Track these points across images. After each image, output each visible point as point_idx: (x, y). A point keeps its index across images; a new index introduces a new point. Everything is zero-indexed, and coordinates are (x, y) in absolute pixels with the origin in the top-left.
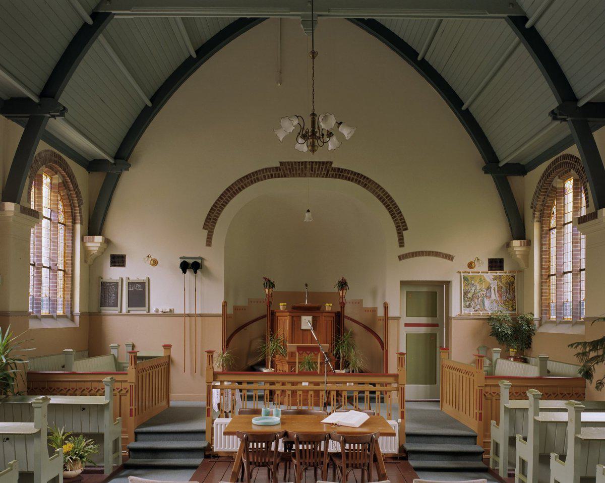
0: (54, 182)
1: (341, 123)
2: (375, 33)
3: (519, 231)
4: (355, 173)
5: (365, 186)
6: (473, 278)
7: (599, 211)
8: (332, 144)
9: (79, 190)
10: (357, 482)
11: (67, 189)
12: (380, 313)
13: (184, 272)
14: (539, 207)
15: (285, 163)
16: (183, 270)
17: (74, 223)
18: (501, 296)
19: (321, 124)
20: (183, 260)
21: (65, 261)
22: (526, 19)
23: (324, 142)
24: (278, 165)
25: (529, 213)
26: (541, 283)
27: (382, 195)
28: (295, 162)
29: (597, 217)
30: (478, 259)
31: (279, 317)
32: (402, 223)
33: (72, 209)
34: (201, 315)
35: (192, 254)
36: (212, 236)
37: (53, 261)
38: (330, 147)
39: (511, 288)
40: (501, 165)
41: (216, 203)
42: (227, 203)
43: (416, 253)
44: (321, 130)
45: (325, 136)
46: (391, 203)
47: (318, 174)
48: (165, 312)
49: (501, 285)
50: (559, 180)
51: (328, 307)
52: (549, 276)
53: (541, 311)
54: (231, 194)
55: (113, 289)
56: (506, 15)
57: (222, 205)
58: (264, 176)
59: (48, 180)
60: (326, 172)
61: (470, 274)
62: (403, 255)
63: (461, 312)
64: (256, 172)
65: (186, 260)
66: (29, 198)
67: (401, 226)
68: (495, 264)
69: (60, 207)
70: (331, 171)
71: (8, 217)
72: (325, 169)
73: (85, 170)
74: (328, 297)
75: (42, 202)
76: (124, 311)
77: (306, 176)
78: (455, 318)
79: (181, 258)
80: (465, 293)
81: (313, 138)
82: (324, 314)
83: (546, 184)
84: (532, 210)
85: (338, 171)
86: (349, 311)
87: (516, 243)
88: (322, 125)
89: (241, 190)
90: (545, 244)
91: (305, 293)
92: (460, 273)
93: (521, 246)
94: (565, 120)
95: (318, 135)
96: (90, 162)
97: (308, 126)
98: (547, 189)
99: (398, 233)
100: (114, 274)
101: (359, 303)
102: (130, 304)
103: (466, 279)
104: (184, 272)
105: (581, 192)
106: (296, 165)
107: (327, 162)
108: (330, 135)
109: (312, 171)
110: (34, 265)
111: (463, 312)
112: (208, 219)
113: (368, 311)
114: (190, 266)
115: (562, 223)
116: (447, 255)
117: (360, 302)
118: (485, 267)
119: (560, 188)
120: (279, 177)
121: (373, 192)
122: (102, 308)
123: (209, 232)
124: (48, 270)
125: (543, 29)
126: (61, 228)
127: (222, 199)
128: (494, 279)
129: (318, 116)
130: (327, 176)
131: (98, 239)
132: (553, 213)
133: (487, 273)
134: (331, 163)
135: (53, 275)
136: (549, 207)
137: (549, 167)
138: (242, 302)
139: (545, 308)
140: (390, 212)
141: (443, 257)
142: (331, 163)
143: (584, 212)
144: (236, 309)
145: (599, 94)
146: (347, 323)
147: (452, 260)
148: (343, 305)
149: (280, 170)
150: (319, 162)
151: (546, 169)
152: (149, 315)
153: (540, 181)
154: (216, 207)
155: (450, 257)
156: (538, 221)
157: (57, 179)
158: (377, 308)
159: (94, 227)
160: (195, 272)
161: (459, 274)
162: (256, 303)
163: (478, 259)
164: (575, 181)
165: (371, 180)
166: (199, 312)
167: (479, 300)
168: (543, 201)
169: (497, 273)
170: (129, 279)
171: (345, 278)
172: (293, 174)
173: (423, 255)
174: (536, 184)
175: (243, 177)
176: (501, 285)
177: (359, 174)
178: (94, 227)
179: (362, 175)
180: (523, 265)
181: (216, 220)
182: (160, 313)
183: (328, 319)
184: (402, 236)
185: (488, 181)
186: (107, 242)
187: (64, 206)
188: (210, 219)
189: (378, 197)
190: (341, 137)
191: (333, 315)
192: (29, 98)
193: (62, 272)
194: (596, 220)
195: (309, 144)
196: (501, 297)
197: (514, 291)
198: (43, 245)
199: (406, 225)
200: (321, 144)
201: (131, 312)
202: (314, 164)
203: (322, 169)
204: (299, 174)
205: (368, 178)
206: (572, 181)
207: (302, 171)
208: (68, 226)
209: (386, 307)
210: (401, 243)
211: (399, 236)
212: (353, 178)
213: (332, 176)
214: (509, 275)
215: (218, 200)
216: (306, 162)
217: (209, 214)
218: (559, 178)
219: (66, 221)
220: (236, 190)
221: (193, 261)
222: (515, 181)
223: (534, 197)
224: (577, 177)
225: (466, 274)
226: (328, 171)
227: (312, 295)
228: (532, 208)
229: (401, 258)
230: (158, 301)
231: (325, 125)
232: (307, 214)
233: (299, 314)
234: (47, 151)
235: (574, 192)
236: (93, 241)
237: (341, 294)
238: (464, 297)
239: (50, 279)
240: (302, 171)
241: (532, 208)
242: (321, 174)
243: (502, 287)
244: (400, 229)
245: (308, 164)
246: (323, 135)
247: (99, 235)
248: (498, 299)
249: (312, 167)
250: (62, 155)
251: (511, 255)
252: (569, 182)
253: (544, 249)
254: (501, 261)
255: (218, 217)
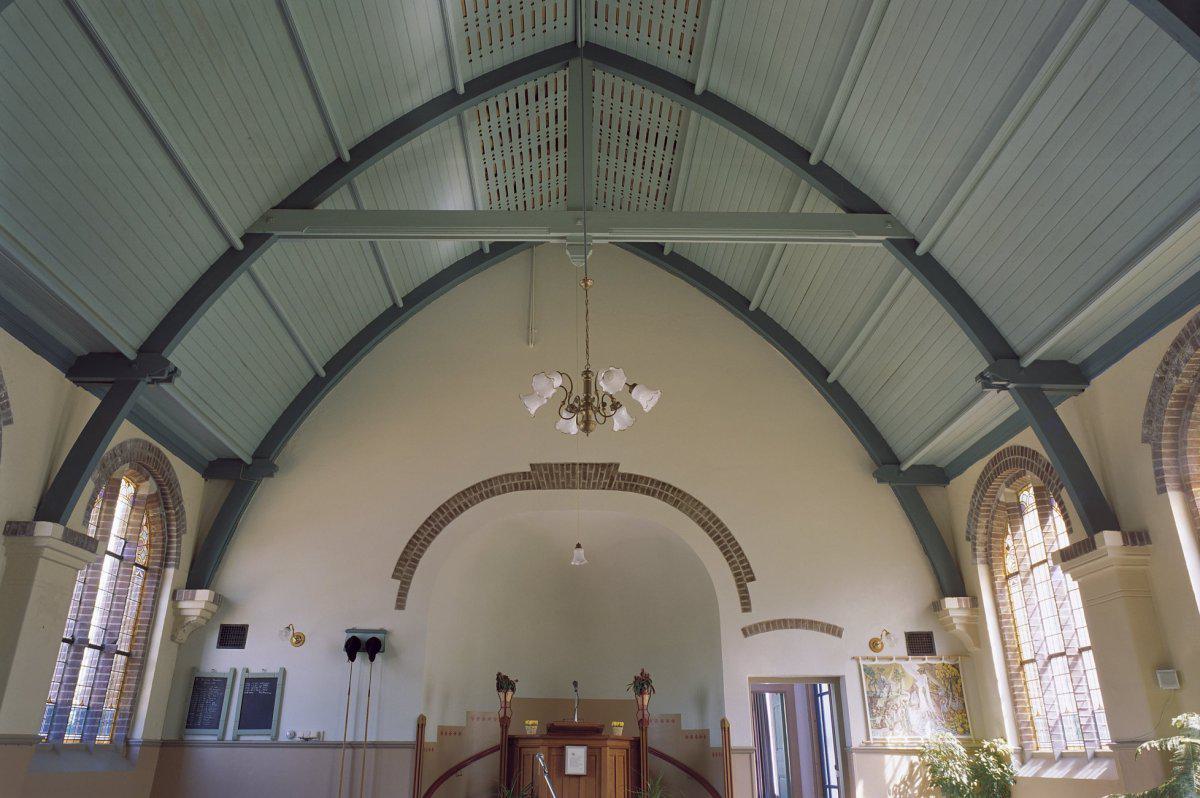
0: (140, 492)
1: (635, 385)
2: (680, 272)
3: (952, 580)
4: (658, 483)
5: (676, 504)
6: (881, 669)
7: (1097, 537)
8: (620, 420)
9: (182, 508)
10: (675, 4)
11: (162, 503)
12: (715, 741)
13: (352, 658)
14: (981, 538)
15: (539, 465)
16: (349, 655)
17: (165, 562)
18: (938, 704)
19: (601, 383)
20: (351, 635)
21: (133, 636)
22: (915, 244)
23: (606, 417)
24: (528, 469)
25: (965, 547)
26: (1011, 679)
27: (706, 519)
28: (556, 465)
29: (1094, 547)
30: (887, 633)
31: (523, 750)
32: (744, 568)
33: (164, 540)
34: (375, 745)
35: (368, 624)
36: (407, 590)
37: (111, 634)
38: (617, 426)
39: (954, 688)
40: (905, 467)
41: (418, 531)
42: (437, 533)
43: (773, 622)
44: (600, 396)
45: (608, 407)
46: (722, 532)
47: (594, 484)
48: (307, 739)
49: (936, 682)
50: (1007, 490)
51: (618, 728)
52: (1022, 663)
53: (1020, 734)
54: (446, 518)
55: (214, 691)
56: (884, 238)
57: (429, 535)
58: (504, 487)
59: (131, 490)
60: (608, 481)
61: (877, 662)
62: (750, 628)
63: (868, 739)
64: (490, 480)
65: (356, 635)
66: (87, 517)
67: (744, 575)
68: (919, 644)
69: (144, 537)
70: (618, 479)
71: (37, 547)
72: (607, 476)
73: (198, 476)
74: (616, 708)
75: (110, 526)
76: (229, 737)
77: (574, 487)
78: (860, 751)
79: (348, 631)
80: (870, 698)
81: (586, 411)
82: (609, 743)
83: (987, 497)
84: (970, 543)
85: (629, 480)
86: (655, 737)
87: (951, 603)
88: (604, 386)
89: (462, 511)
90: (1004, 604)
91: (573, 701)
92: (858, 660)
93: (960, 608)
94: (1004, 388)
95: (595, 404)
96: (210, 462)
97: (579, 391)
98: (989, 506)
99: (739, 586)
100: (223, 662)
101: (673, 721)
102: (245, 723)
103: (869, 671)
104: (352, 658)
105: (1051, 507)
106: (557, 469)
107: (610, 465)
108: (616, 406)
109: (585, 478)
110: (70, 642)
111: (871, 737)
112: (403, 560)
113: (692, 737)
114: (363, 646)
115: (1029, 564)
116: (829, 626)
117: (676, 719)
118: (902, 647)
119: (1013, 504)
120: (528, 488)
121: (691, 514)
122: (188, 731)
123: (403, 583)
124: (97, 651)
125: (945, 256)
126: (139, 575)
127: (429, 525)
128: (922, 672)
129: (595, 374)
130: (610, 487)
131: (203, 595)
132: (1008, 548)
133: (907, 660)
134: (617, 466)
135: (105, 663)
136: (997, 536)
137: (987, 469)
138: (454, 720)
139: (1024, 730)
140: (721, 549)
141: (822, 630)
142: (617, 466)
143: (1064, 542)
144: (443, 732)
145: (1051, 348)
146: (653, 762)
147: (840, 635)
148: (643, 723)
149: (530, 478)
150: (596, 464)
151: (983, 473)
152: (275, 744)
153: (975, 493)
154: (418, 539)
155: (835, 631)
156: (982, 562)
157: (148, 488)
158: (708, 730)
159: (200, 575)
160: (372, 659)
161: (855, 662)
162: (480, 721)
163: (887, 633)
164: (1035, 489)
165: (685, 494)
166: (371, 738)
167: (899, 711)
168: (987, 527)
169: (924, 659)
170: (247, 671)
171: (646, 671)
172: (553, 484)
173: (786, 627)
174: (969, 499)
175: (468, 489)
176: (936, 682)
177: (664, 484)
178: (200, 575)
179: (670, 486)
180: (967, 639)
181: (417, 562)
182: (297, 739)
183: (617, 752)
184: (746, 591)
185: (884, 499)
186: (219, 600)
187: (150, 534)
188: (406, 561)
189: (699, 522)
190: (635, 408)
191: (627, 744)
192: (121, 354)
193: (124, 657)
194: (1094, 552)
195: (580, 420)
196: (939, 706)
197: (961, 695)
198: (97, 604)
199: (751, 572)
200: (601, 419)
201: (242, 738)
202: (588, 467)
203: (602, 475)
204: (563, 483)
205: (680, 491)
206: (1032, 490)
207: (568, 477)
208: (153, 571)
209: (725, 729)
210: (746, 605)
211: (740, 592)
212: (655, 490)
213: (620, 488)
214: (946, 662)
215: (422, 527)
216: (574, 464)
217: (404, 552)
218: (1008, 486)
219: (151, 561)
220: (455, 510)
221: (370, 636)
222: (931, 495)
223: (969, 521)
224: (1041, 484)
225: (869, 663)
226: (612, 479)
227: (586, 705)
228: (968, 539)
229: (747, 632)
230: (295, 718)
231: (610, 384)
232: (576, 551)
233: (559, 743)
234: (137, 440)
235: (1039, 510)
236: (193, 599)
237: (640, 703)
238: (871, 708)
239: (97, 669)
240: (568, 477)
241: (968, 539)
242: (600, 483)
243: (937, 687)
244: (741, 580)
245: (577, 467)
246: (604, 404)
247: (206, 588)
248: (934, 710)
249: (585, 473)
250: (162, 448)
251: (947, 626)
252: (1026, 493)
253: (1003, 613)
254: (929, 636)
255: (420, 557)
